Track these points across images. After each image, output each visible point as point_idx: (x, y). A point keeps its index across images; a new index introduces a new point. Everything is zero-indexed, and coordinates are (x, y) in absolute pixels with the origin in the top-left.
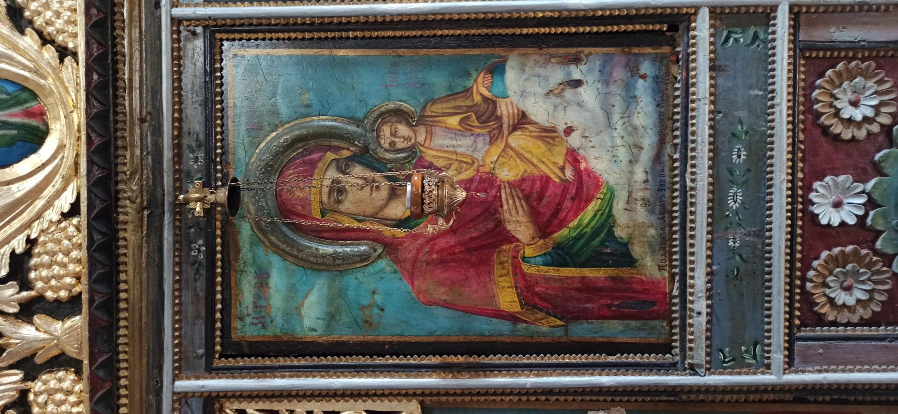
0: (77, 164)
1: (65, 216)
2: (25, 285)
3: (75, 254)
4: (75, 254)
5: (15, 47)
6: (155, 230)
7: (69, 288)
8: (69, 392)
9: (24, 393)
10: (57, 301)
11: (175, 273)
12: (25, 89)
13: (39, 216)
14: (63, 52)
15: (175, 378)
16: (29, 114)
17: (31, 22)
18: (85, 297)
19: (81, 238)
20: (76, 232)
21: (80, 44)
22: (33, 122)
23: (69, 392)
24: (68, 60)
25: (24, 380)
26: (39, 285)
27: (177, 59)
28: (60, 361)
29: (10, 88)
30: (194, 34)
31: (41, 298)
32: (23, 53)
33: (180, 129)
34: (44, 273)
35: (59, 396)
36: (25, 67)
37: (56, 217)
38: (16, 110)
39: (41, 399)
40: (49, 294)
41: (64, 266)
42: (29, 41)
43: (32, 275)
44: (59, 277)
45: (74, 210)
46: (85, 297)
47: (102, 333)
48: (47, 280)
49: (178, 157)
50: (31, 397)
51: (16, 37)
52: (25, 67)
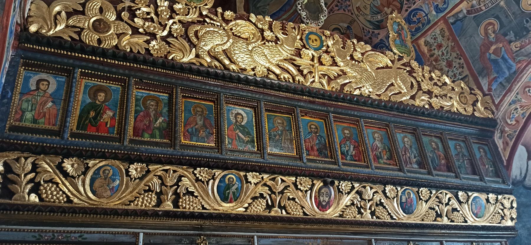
0: (217, 210)
1: (203, 206)
2: (184, 195)
3: (192, 208)
4: (192, 208)
5: (248, 197)
6: (194, 229)
7: (182, 205)
8: (150, 203)
9: (152, 192)
10: (178, 202)
11: (31, 230)
12: (237, 198)
13: (203, 199)
14: (246, 208)
15: (144, 233)
16: (231, 199)
17: (254, 201)
18: (179, 210)
19: (196, 210)
20: (198, 209)
21: (249, 212)
22: (229, 200)
23: (150, 203)
24: (244, 210)
25: (156, 192)
26: (184, 198)
27: (124, 233)
28: (159, 202)
29: (238, 195)
30: (249, 242)
31: (180, 198)
32: (246, 199)
33: (223, 237)
34: (187, 199)
35: (149, 201)
36: (243, 199)
37: (203, 204)
38: (232, 196)
39: (150, 196)
40: (181, 200)
41: (189, 204)
42: (250, 201)
43: (187, 196)
44: (186, 203)
45: (204, 208)
46: (179, 210)
47: (167, 214)
48: (185, 200)
49: (214, 236)
50: (150, 193)
51: (250, 197)
52: (243, 199)
